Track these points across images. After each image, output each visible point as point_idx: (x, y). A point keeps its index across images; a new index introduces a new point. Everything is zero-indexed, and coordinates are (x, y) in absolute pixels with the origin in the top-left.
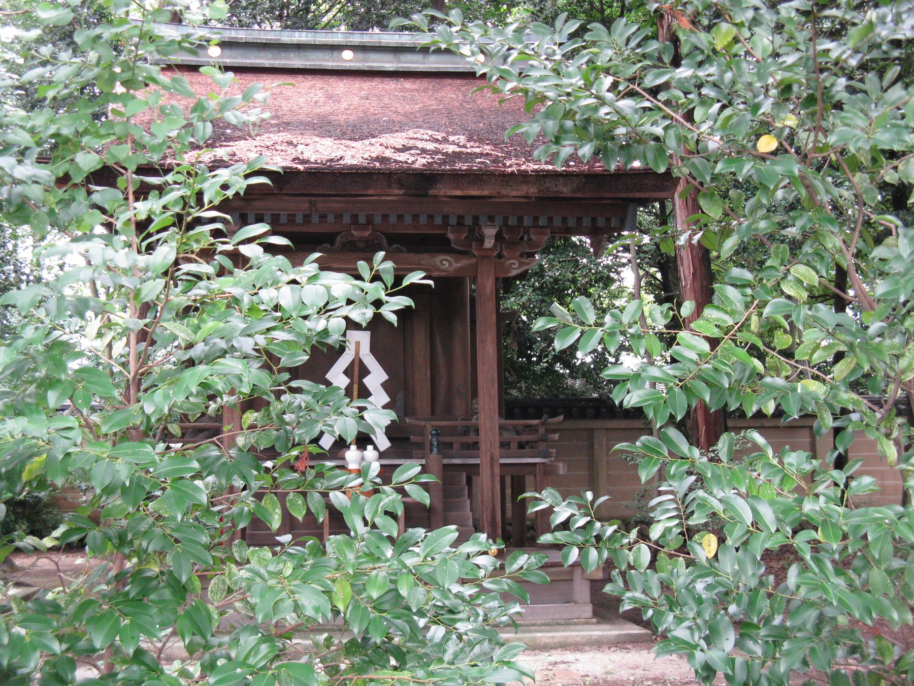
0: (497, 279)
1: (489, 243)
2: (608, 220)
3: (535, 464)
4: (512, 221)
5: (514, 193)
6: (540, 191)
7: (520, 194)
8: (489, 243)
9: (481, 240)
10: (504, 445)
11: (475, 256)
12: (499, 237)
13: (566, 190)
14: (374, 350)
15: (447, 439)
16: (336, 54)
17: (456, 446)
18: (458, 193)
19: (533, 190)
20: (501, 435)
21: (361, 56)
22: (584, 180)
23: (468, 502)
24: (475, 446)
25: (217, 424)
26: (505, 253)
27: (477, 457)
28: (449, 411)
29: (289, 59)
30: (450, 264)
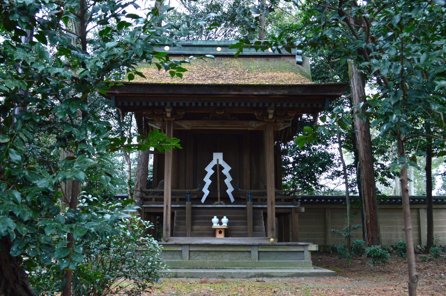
0: (274, 131)
1: (271, 116)
2: (318, 105)
3: (291, 208)
4: (279, 105)
5: (279, 93)
6: (289, 92)
7: (281, 93)
8: (271, 116)
9: (267, 115)
10: (276, 200)
11: (265, 122)
12: (275, 115)
13: (299, 92)
14: (225, 159)
15: (255, 197)
16: (214, 48)
17: (259, 200)
18: (256, 93)
19: (286, 92)
20: (275, 196)
21: (224, 49)
22: (269, 7)
23: (263, 222)
24: (266, 200)
25: (195, 206)
26: (277, 121)
27: (266, 204)
28: (257, 187)
29: (196, 51)
30: (255, 125)
